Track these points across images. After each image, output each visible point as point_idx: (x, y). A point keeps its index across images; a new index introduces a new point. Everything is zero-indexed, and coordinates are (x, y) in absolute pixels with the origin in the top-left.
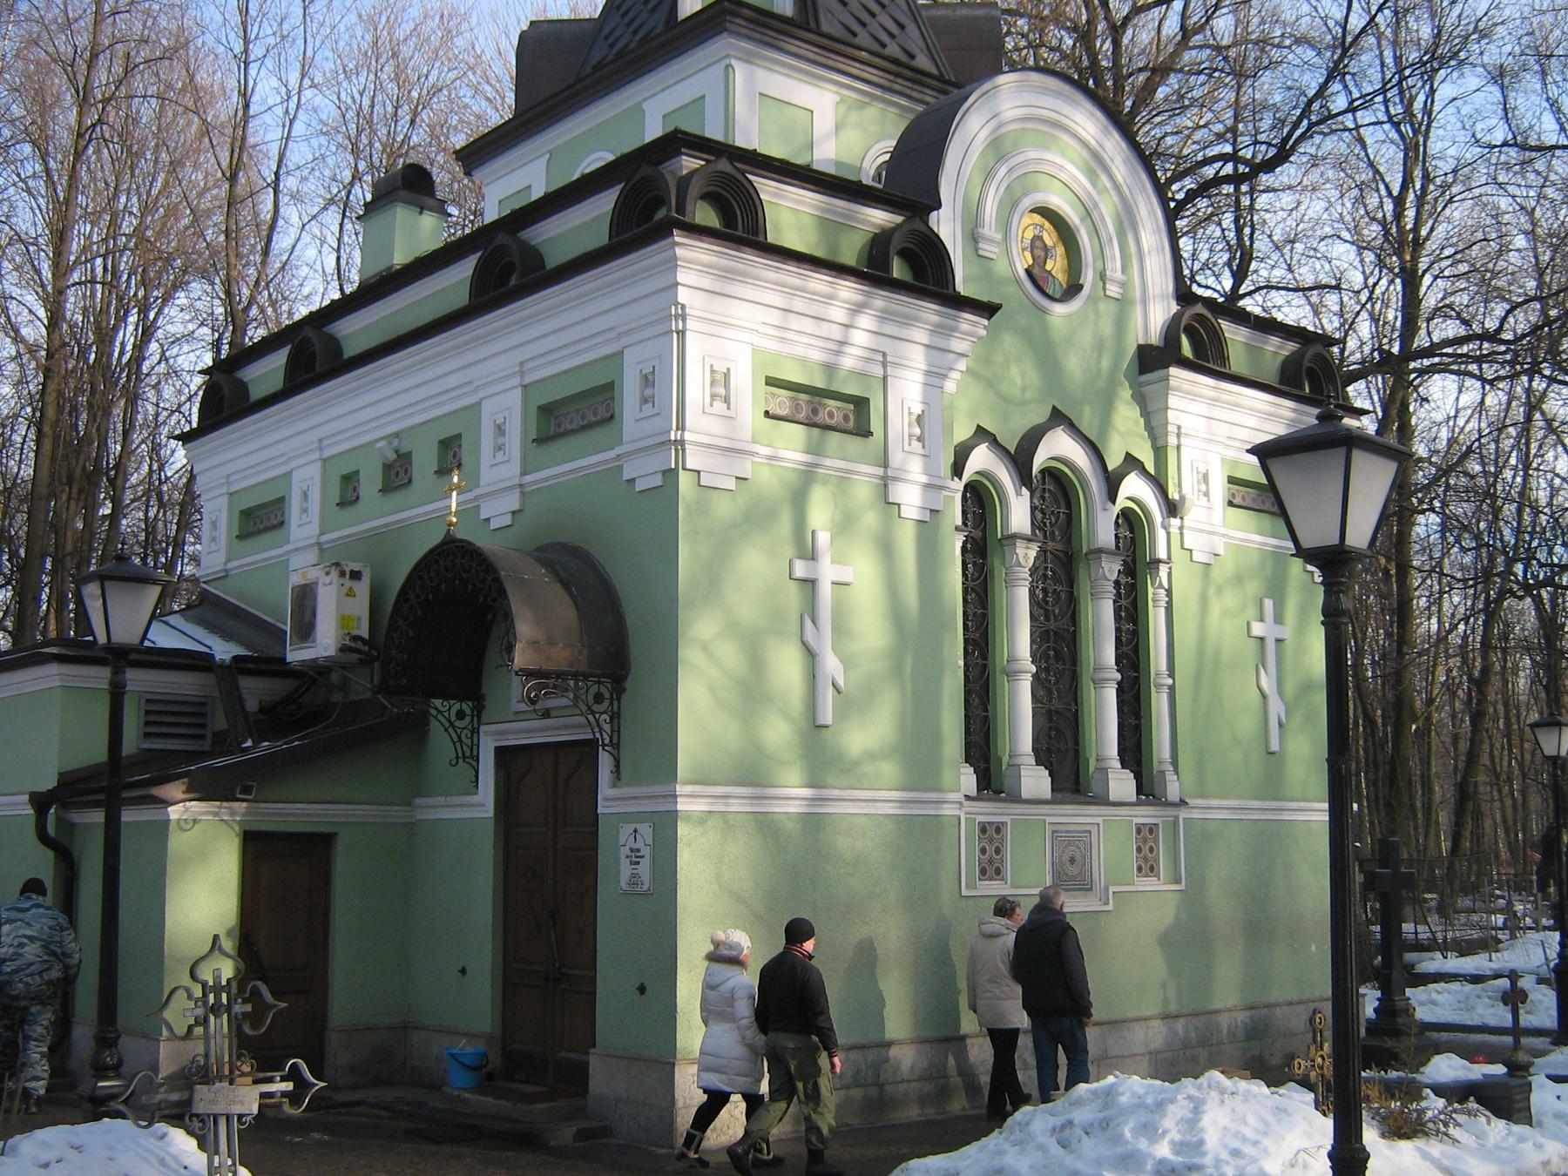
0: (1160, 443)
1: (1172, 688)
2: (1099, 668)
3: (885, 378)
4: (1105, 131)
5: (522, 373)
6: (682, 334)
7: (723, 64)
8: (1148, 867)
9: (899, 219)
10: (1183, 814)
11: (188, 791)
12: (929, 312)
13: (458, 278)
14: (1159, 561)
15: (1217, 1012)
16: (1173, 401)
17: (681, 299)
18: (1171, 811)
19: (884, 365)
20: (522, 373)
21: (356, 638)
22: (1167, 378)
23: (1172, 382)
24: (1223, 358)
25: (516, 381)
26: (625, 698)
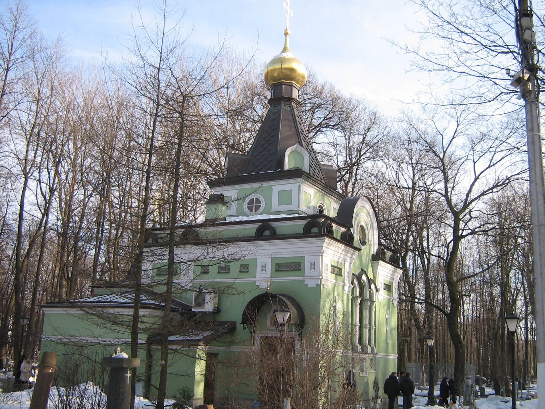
0: (375, 276)
1: (375, 329)
2: (366, 325)
3: (344, 264)
4: (370, 208)
5: (272, 255)
6: (322, 256)
7: (299, 184)
8: (371, 368)
9: (346, 230)
10: (377, 356)
11: (204, 343)
12: (351, 250)
13: (252, 229)
14: (374, 302)
15: (197, 399)
16: (379, 267)
17: (323, 249)
18: (375, 356)
19: (345, 261)
20: (272, 255)
21: (216, 308)
22: (378, 263)
23: (380, 264)
24: (332, 234)
25: (270, 256)
26: (304, 330)
